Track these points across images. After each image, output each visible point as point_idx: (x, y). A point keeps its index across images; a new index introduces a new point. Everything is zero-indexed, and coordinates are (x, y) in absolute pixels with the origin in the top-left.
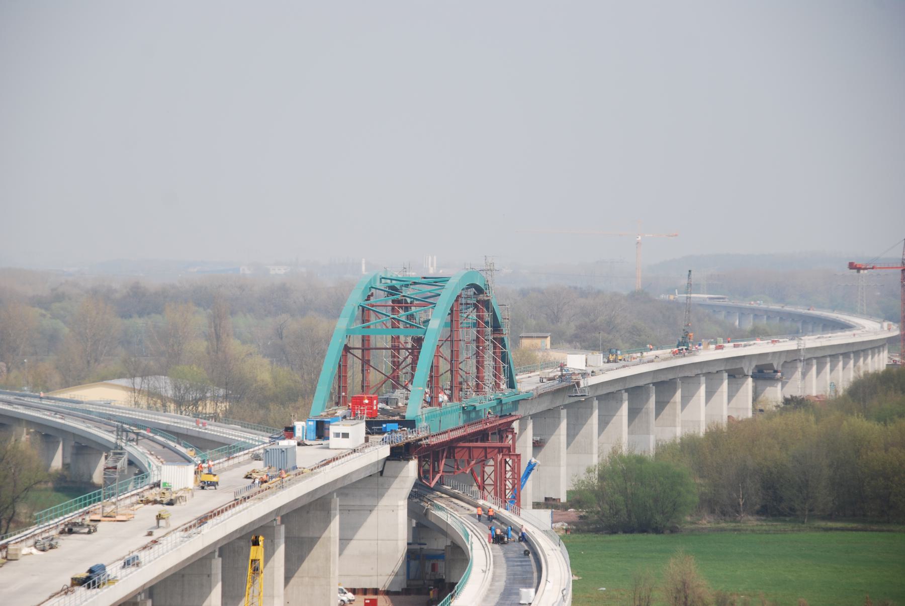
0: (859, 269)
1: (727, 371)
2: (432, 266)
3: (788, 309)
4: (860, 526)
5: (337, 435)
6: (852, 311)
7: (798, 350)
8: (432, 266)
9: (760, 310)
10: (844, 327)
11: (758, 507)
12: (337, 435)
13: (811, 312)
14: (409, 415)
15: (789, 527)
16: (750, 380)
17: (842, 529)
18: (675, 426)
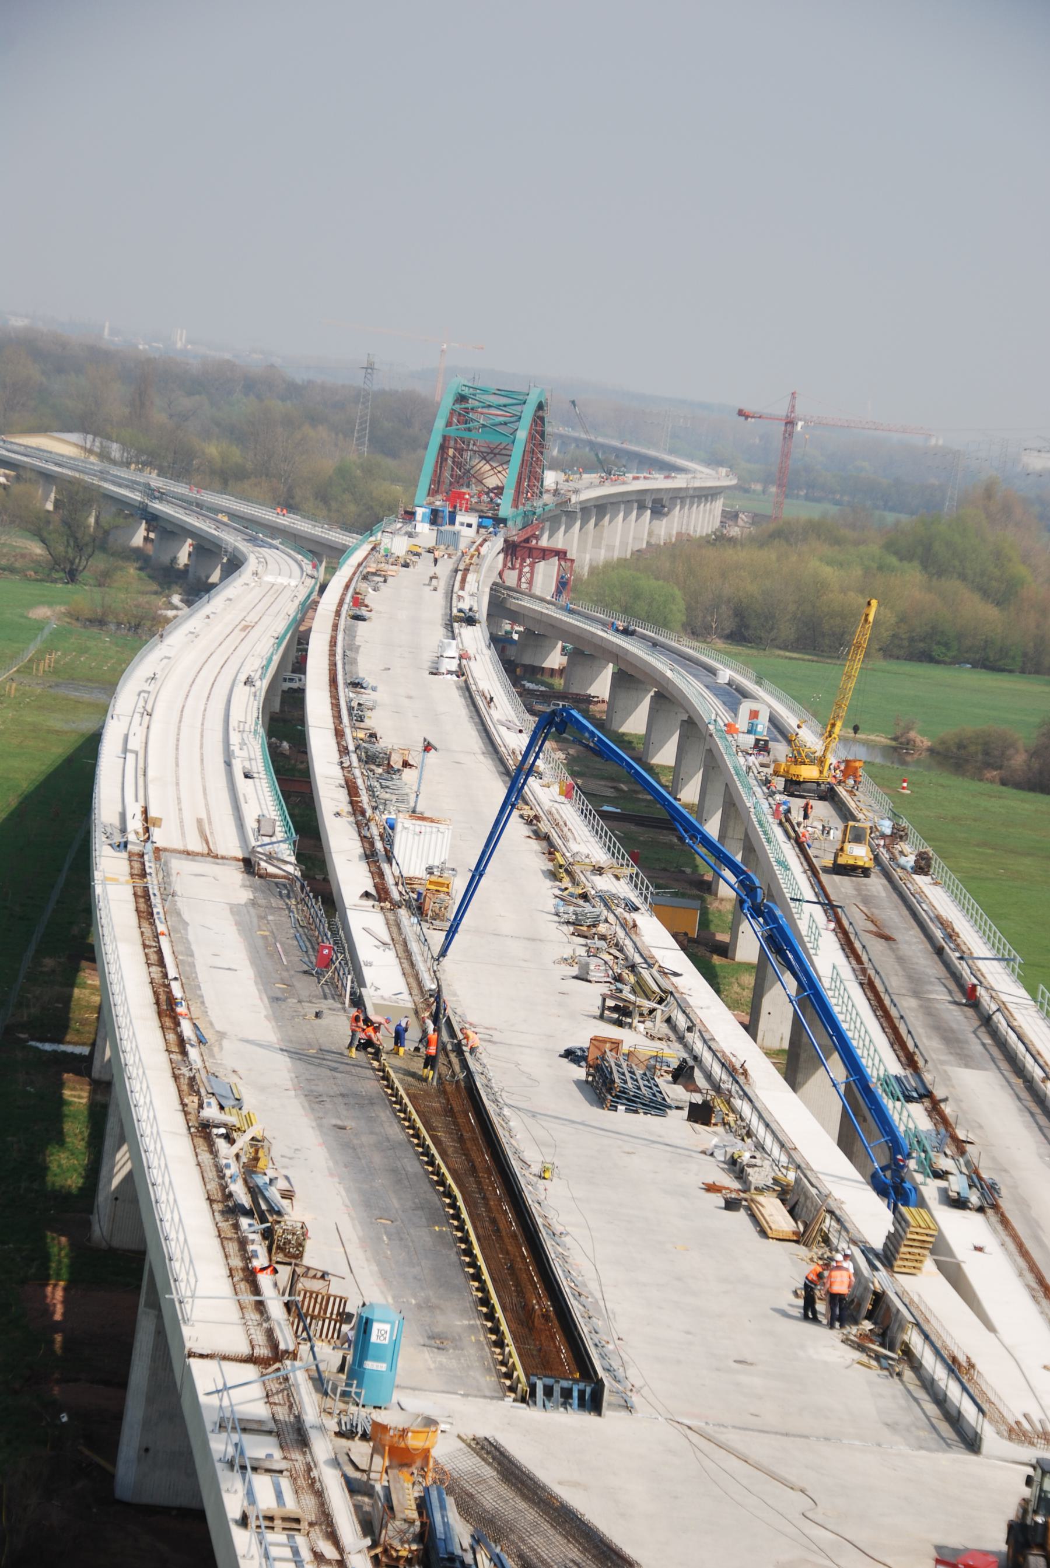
0: (747, 417)
1: (637, 501)
2: (181, 339)
3: (600, 440)
4: (815, 658)
5: (462, 524)
6: (691, 458)
7: (687, 489)
8: (181, 339)
9: (568, 437)
10: (669, 469)
11: (728, 631)
12: (462, 524)
13: (624, 446)
14: (502, 513)
15: (754, 652)
16: (649, 512)
17: (809, 660)
18: (600, 548)
